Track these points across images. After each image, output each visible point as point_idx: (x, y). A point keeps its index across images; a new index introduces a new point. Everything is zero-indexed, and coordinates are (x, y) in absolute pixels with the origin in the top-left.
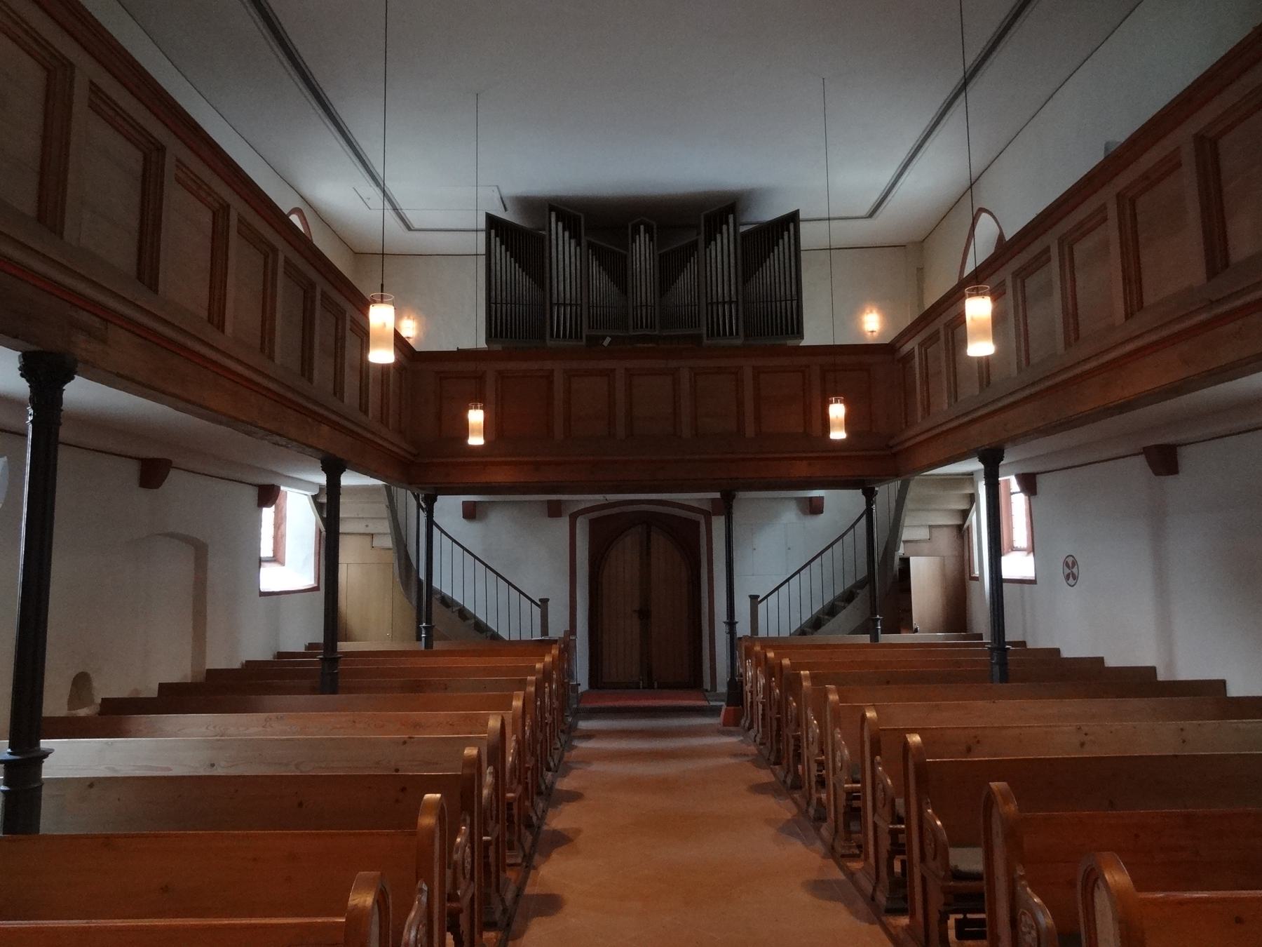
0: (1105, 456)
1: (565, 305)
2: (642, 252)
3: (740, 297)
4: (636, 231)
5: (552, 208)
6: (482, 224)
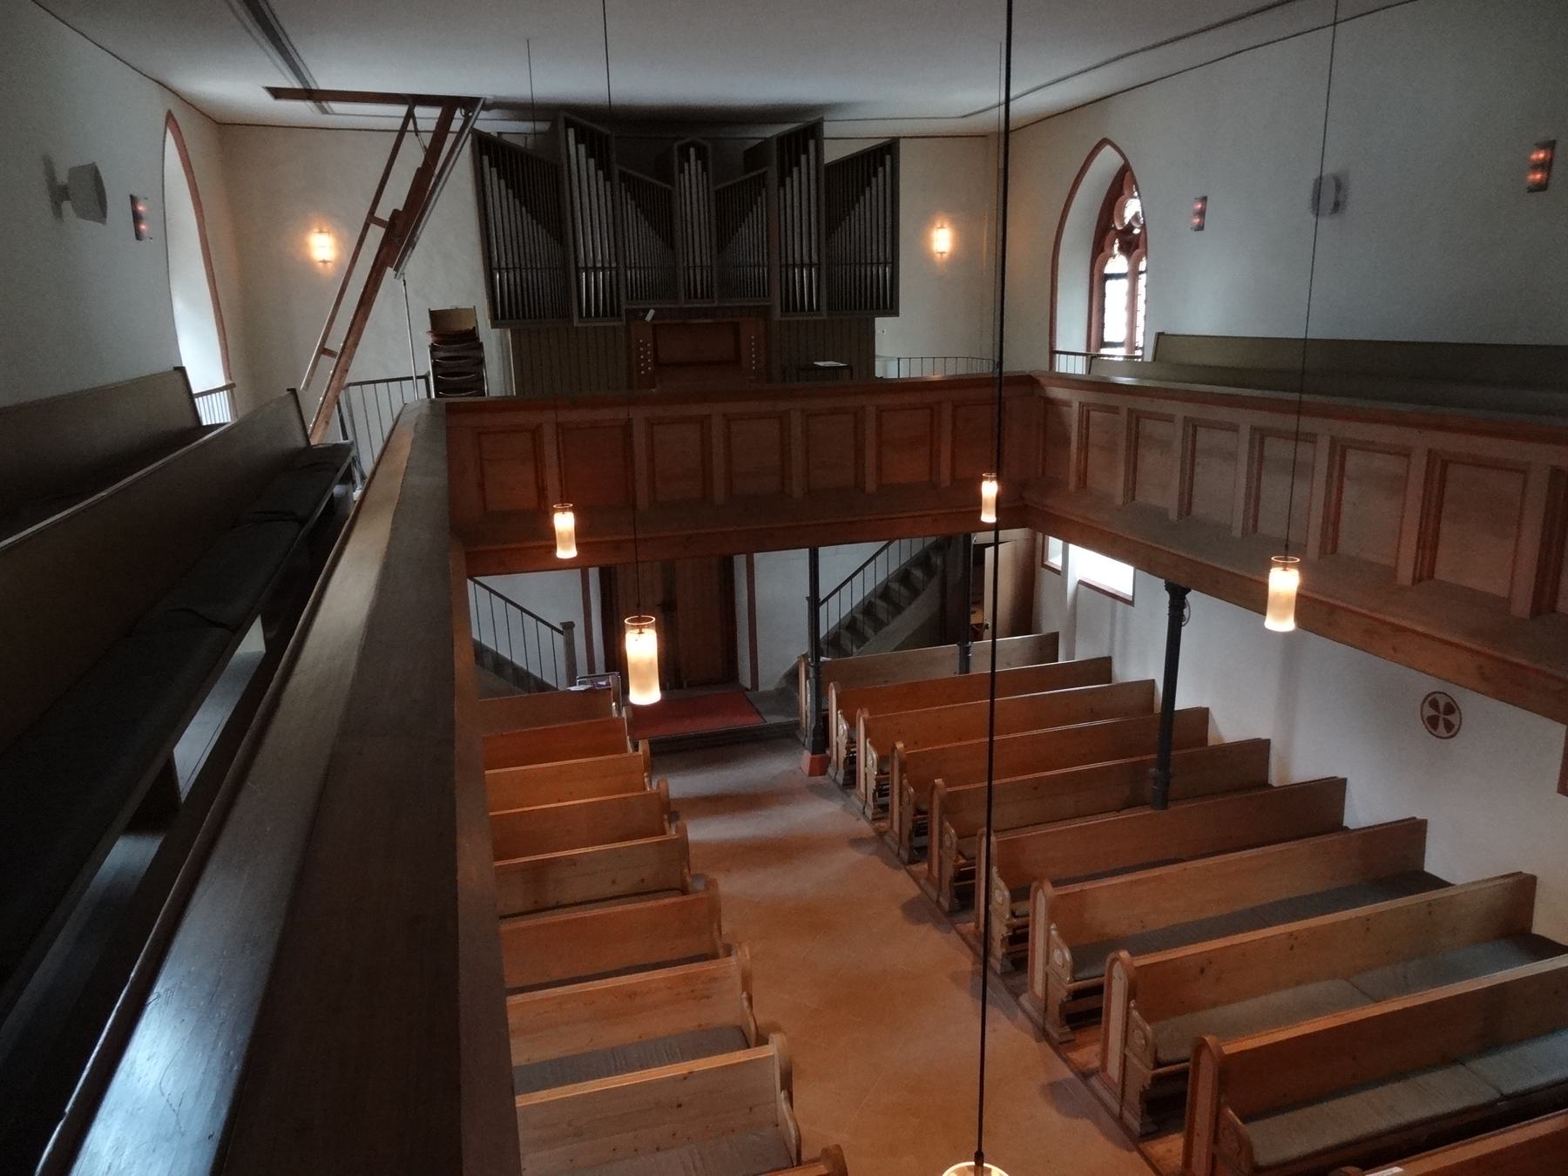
1: (595, 269)
2: (692, 188)
3: (823, 260)
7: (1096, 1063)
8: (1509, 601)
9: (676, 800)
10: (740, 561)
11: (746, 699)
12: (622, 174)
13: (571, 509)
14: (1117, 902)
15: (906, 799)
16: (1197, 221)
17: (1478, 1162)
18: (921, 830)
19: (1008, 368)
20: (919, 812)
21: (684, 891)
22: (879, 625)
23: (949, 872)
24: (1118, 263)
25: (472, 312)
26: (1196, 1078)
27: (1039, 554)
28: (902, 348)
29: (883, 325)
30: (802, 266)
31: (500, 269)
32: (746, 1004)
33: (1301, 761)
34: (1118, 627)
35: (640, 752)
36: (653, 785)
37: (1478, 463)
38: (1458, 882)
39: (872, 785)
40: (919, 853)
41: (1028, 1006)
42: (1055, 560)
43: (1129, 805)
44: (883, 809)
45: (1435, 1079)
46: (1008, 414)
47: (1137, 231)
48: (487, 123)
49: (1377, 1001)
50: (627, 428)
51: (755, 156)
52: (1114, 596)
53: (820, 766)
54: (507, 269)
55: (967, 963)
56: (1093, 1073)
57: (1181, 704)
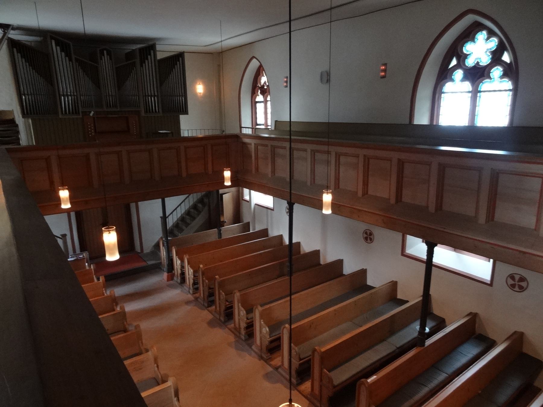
0: (211, 46)
1: (67, 95)
2: (106, 65)
3: (159, 93)
7: (280, 364)
8: (389, 199)
9: (118, 297)
10: (133, 206)
11: (139, 257)
12: (76, 58)
13: (67, 189)
14: (280, 309)
15: (205, 285)
16: (285, 84)
18: (211, 294)
20: (210, 288)
21: (125, 331)
22: (187, 225)
23: (223, 308)
24: (260, 98)
25: (11, 112)
26: (313, 361)
27: (241, 195)
28: (190, 126)
29: (182, 117)
30: (151, 96)
31: (24, 95)
32: (156, 369)
33: (329, 256)
34: (269, 219)
35: (101, 281)
36: (108, 293)
37: (377, 158)
38: (377, 287)
39: (192, 281)
40: (211, 303)
41: (255, 349)
42: (247, 197)
43: (279, 276)
44: (196, 290)
45: (379, 347)
46: (228, 148)
47: (265, 87)
48: (13, 35)
49: (361, 326)
50: (87, 157)
51: (130, 55)
52: (267, 208)
53: (171, 277)
54: (28, 95)
55: (232, 338)
56: (280, 367)
57: (294, 241)
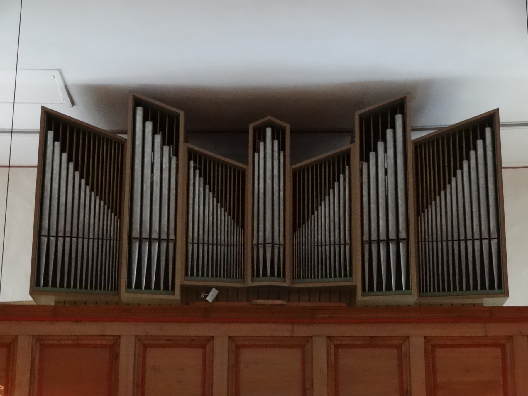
1: (150, 240)
2: (268, 167)
4: (260, 135)
5: (138, 102)
6: (35, 122)
17: (291, 147)
19: (503, 169)
50: (113, 347)
